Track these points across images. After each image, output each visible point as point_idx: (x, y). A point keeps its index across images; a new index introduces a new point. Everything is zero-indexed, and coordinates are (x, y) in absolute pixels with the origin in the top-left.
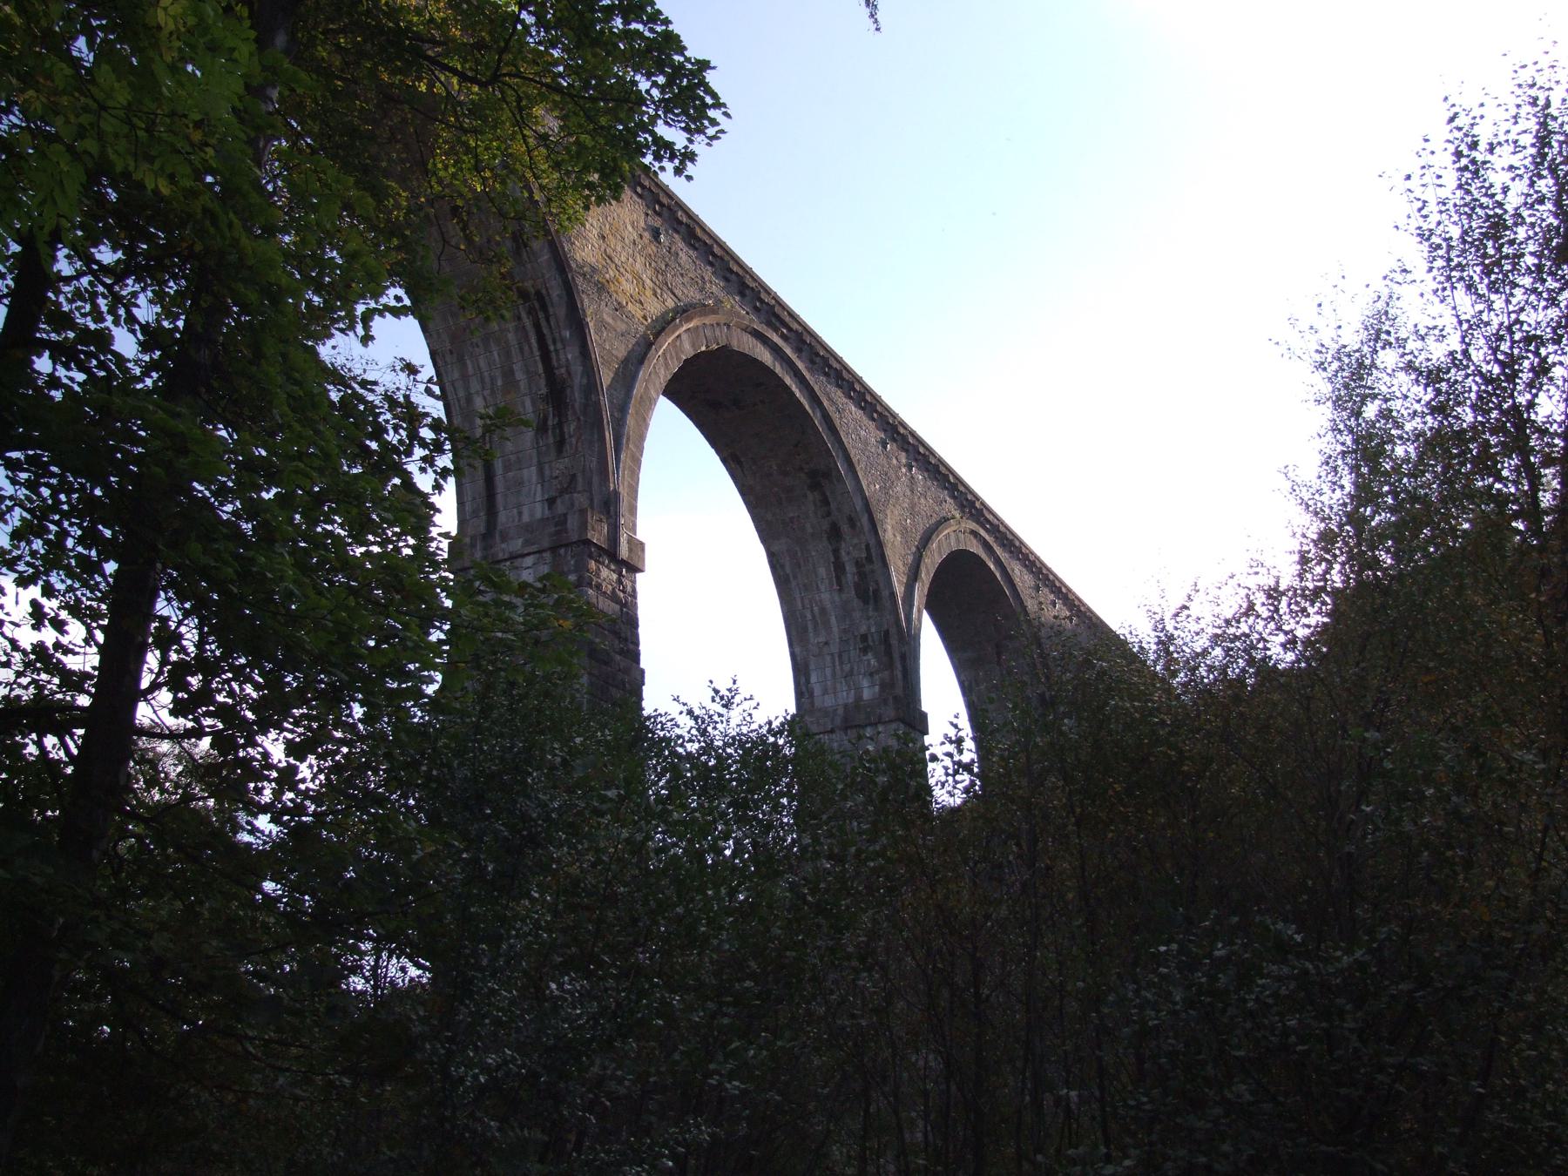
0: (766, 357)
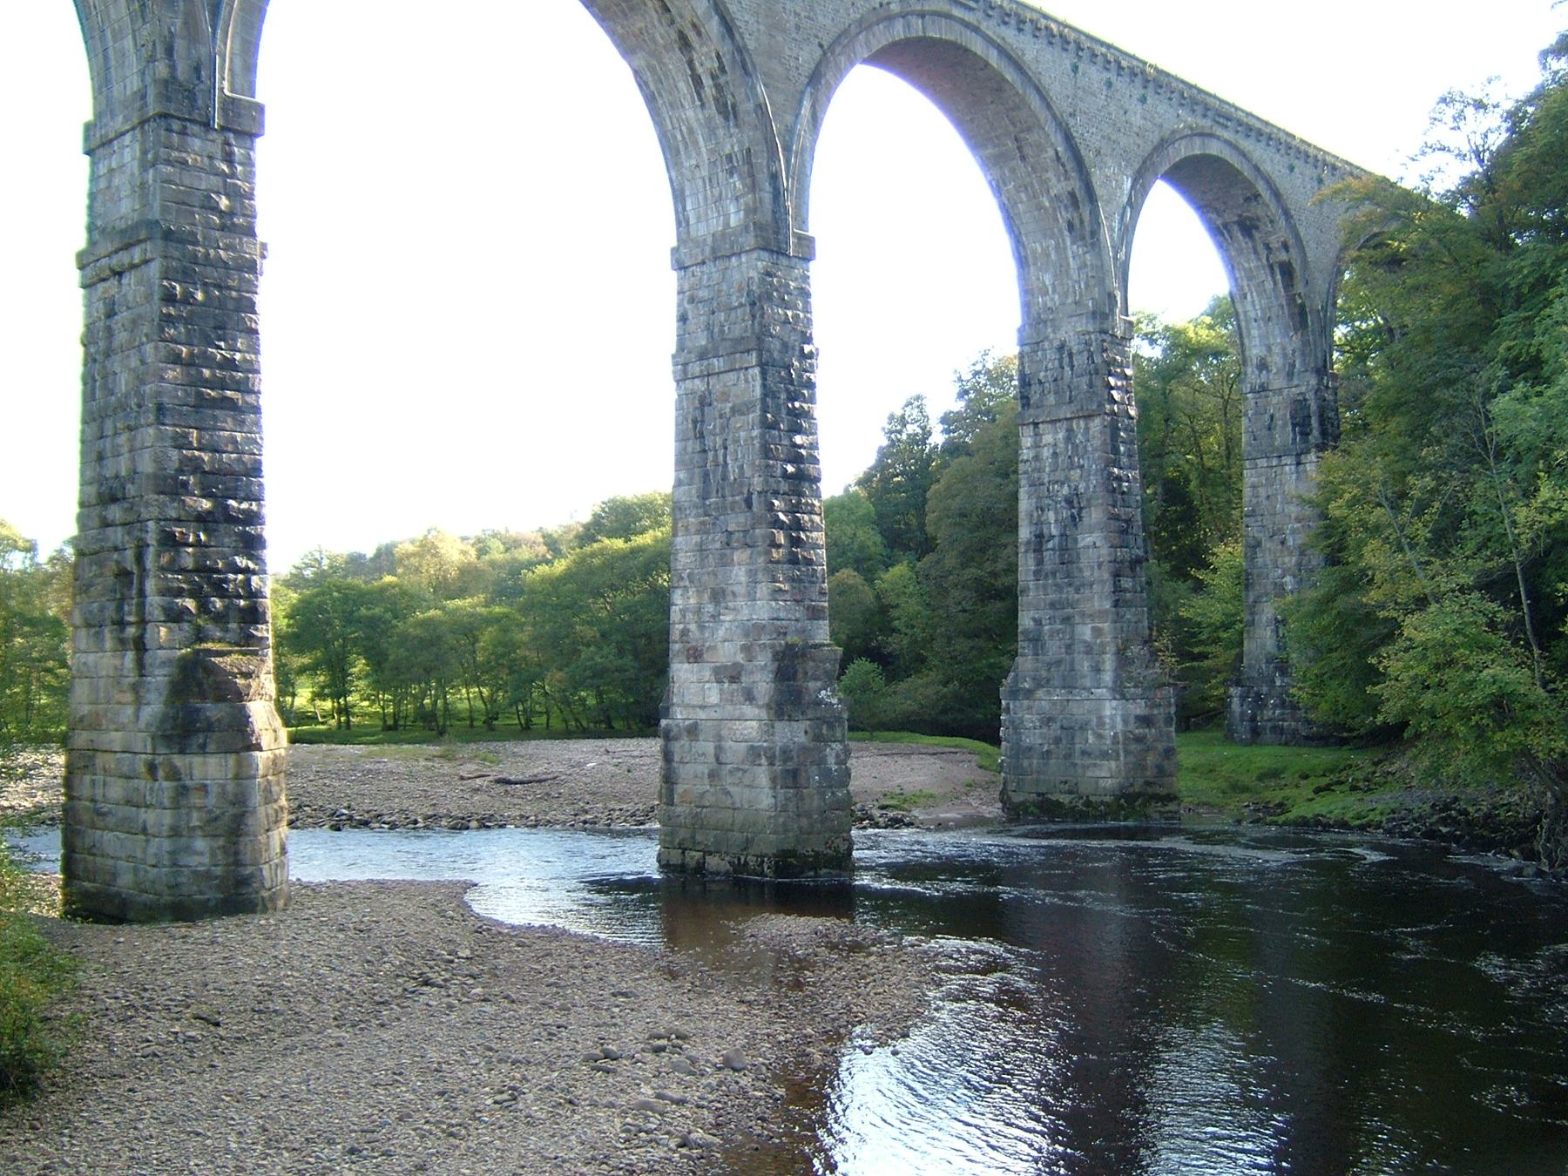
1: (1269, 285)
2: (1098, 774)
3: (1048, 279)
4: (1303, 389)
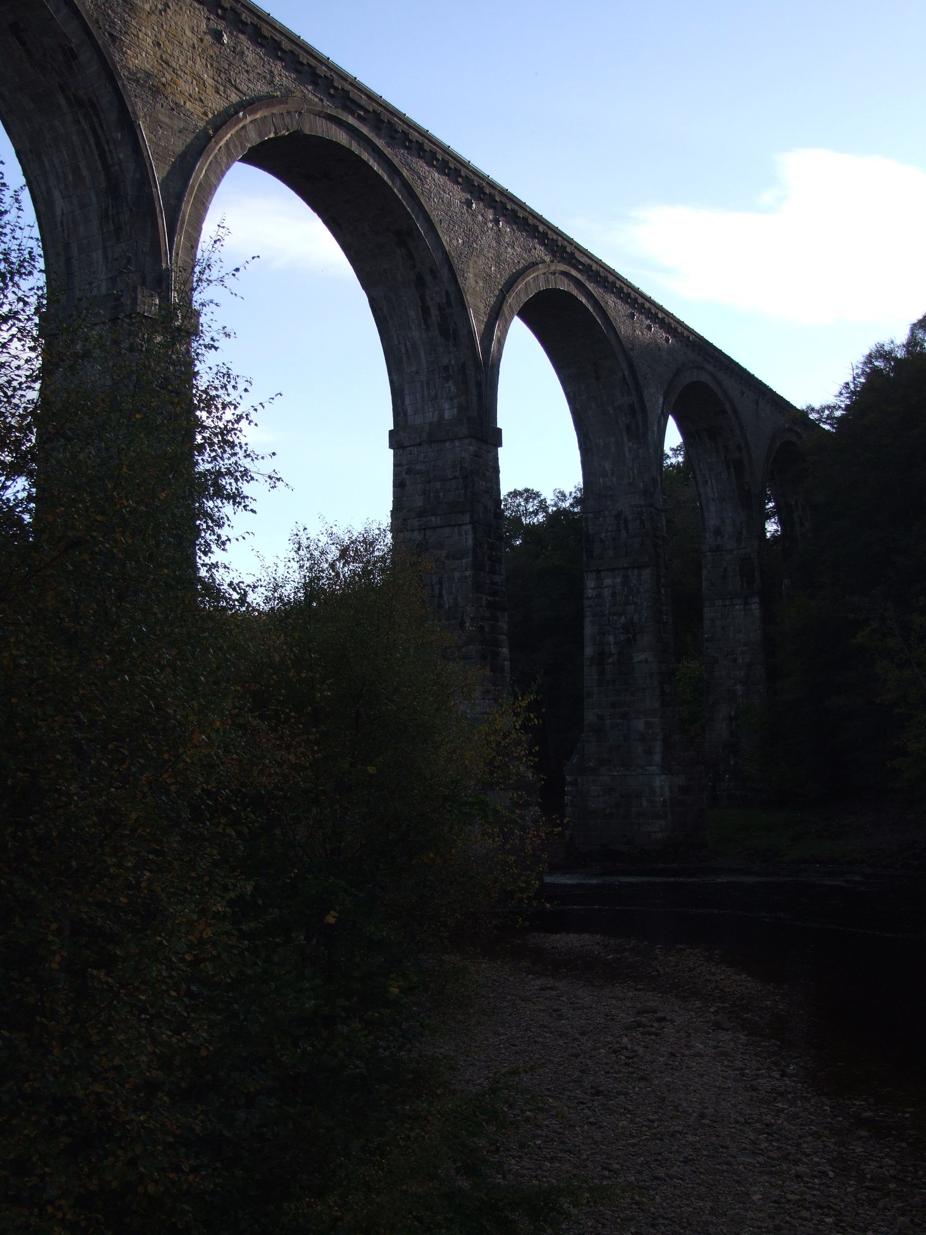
0: (342, 138)
3: (608, 466)
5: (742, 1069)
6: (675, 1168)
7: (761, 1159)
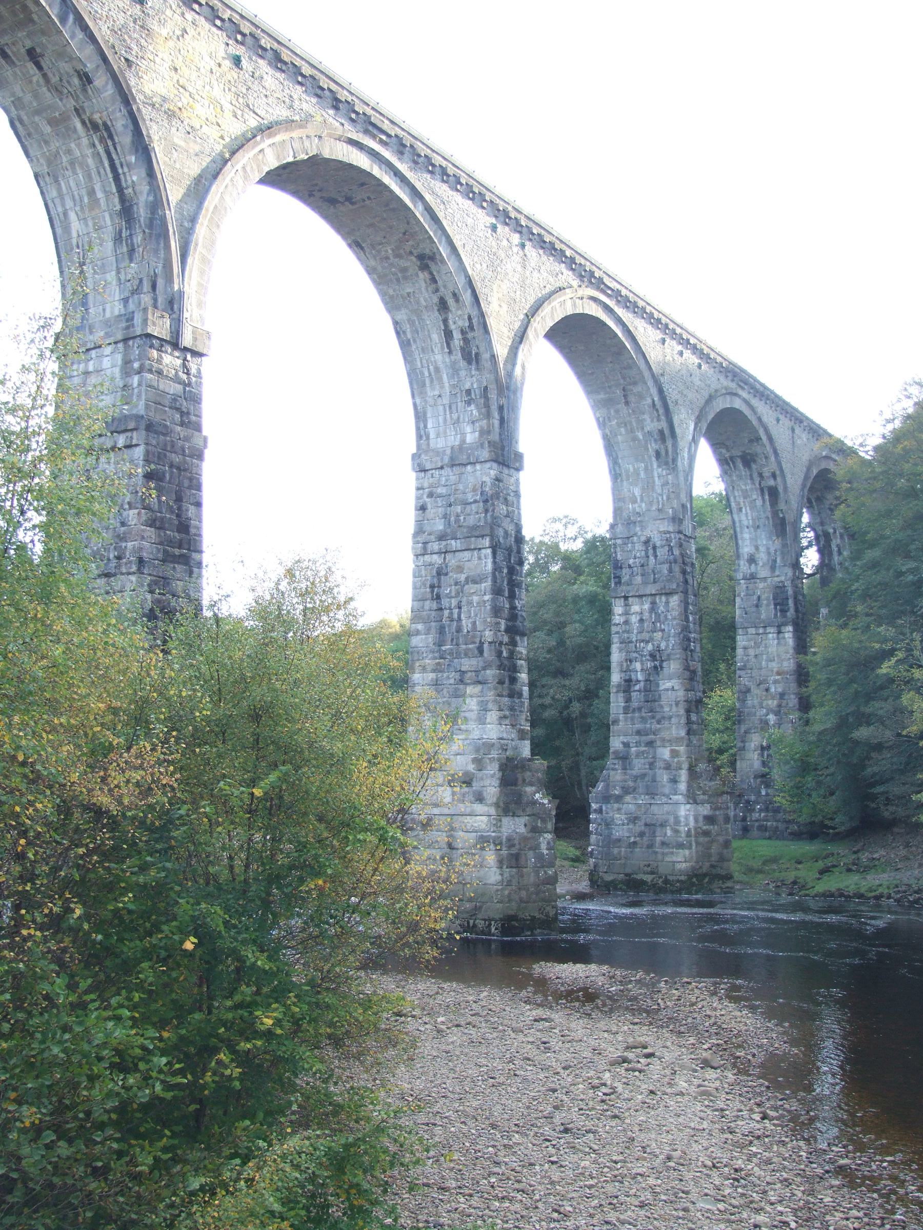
0: (361, 161)
1: (759, 503)
2: (675, 859)
3: (637, 492)
4: (783, 578)
5: (722, 1110)
6: (629, 1213)
7: (721, 1206)
